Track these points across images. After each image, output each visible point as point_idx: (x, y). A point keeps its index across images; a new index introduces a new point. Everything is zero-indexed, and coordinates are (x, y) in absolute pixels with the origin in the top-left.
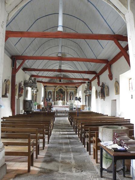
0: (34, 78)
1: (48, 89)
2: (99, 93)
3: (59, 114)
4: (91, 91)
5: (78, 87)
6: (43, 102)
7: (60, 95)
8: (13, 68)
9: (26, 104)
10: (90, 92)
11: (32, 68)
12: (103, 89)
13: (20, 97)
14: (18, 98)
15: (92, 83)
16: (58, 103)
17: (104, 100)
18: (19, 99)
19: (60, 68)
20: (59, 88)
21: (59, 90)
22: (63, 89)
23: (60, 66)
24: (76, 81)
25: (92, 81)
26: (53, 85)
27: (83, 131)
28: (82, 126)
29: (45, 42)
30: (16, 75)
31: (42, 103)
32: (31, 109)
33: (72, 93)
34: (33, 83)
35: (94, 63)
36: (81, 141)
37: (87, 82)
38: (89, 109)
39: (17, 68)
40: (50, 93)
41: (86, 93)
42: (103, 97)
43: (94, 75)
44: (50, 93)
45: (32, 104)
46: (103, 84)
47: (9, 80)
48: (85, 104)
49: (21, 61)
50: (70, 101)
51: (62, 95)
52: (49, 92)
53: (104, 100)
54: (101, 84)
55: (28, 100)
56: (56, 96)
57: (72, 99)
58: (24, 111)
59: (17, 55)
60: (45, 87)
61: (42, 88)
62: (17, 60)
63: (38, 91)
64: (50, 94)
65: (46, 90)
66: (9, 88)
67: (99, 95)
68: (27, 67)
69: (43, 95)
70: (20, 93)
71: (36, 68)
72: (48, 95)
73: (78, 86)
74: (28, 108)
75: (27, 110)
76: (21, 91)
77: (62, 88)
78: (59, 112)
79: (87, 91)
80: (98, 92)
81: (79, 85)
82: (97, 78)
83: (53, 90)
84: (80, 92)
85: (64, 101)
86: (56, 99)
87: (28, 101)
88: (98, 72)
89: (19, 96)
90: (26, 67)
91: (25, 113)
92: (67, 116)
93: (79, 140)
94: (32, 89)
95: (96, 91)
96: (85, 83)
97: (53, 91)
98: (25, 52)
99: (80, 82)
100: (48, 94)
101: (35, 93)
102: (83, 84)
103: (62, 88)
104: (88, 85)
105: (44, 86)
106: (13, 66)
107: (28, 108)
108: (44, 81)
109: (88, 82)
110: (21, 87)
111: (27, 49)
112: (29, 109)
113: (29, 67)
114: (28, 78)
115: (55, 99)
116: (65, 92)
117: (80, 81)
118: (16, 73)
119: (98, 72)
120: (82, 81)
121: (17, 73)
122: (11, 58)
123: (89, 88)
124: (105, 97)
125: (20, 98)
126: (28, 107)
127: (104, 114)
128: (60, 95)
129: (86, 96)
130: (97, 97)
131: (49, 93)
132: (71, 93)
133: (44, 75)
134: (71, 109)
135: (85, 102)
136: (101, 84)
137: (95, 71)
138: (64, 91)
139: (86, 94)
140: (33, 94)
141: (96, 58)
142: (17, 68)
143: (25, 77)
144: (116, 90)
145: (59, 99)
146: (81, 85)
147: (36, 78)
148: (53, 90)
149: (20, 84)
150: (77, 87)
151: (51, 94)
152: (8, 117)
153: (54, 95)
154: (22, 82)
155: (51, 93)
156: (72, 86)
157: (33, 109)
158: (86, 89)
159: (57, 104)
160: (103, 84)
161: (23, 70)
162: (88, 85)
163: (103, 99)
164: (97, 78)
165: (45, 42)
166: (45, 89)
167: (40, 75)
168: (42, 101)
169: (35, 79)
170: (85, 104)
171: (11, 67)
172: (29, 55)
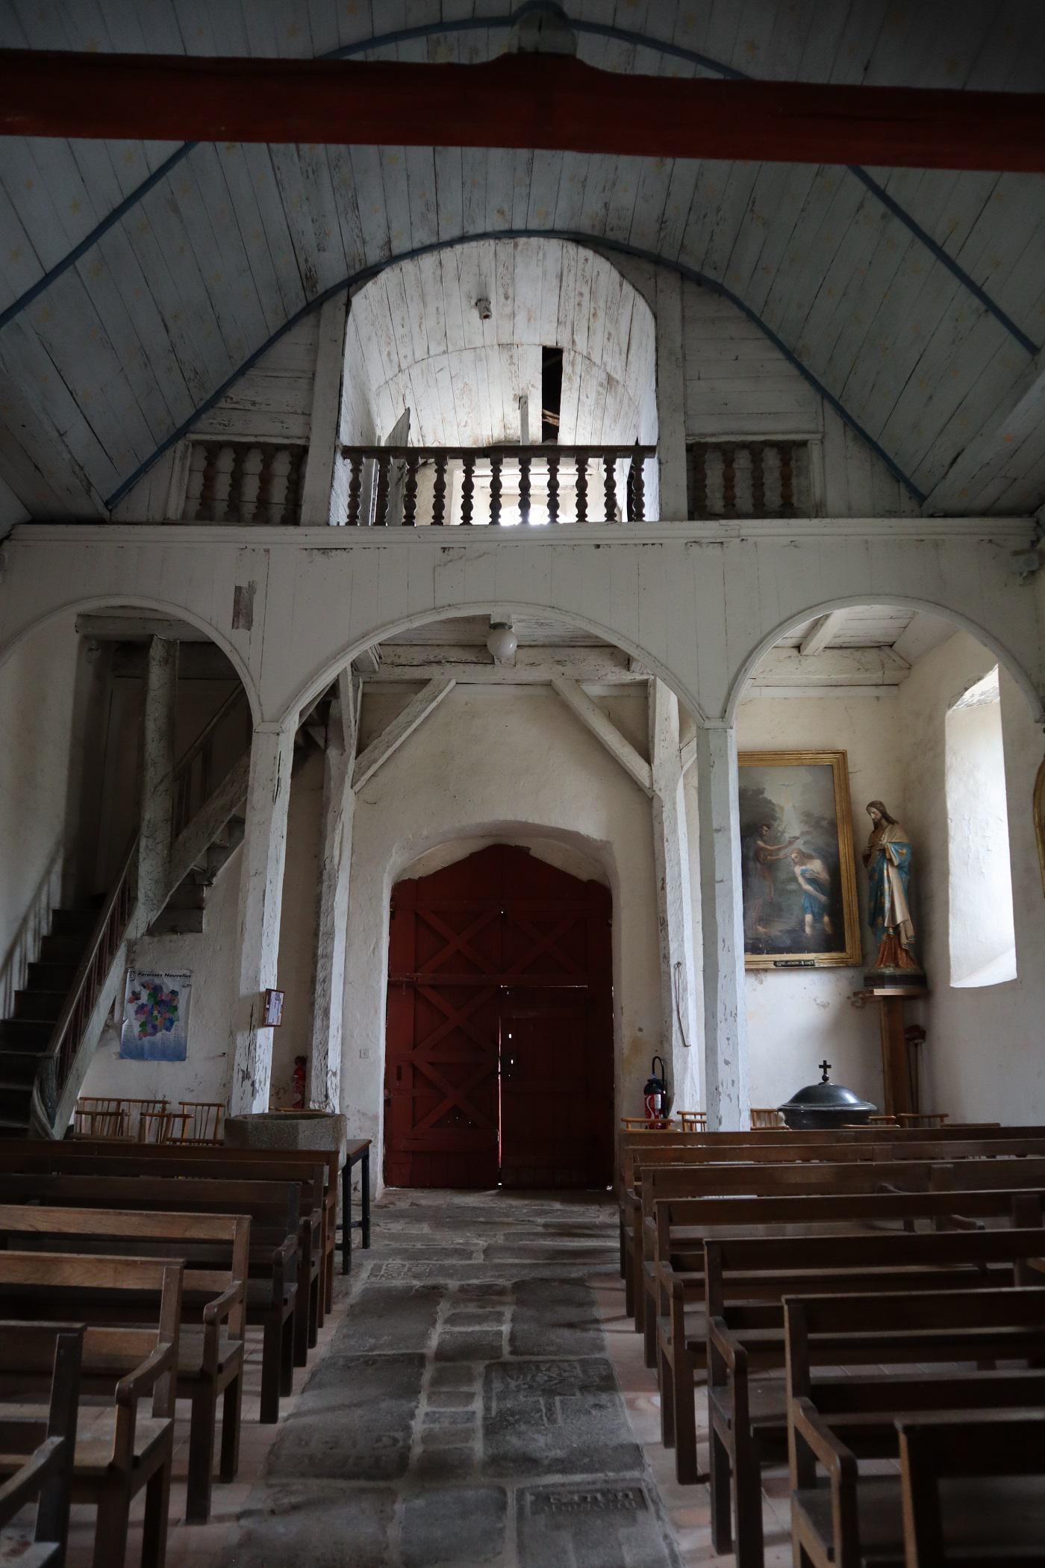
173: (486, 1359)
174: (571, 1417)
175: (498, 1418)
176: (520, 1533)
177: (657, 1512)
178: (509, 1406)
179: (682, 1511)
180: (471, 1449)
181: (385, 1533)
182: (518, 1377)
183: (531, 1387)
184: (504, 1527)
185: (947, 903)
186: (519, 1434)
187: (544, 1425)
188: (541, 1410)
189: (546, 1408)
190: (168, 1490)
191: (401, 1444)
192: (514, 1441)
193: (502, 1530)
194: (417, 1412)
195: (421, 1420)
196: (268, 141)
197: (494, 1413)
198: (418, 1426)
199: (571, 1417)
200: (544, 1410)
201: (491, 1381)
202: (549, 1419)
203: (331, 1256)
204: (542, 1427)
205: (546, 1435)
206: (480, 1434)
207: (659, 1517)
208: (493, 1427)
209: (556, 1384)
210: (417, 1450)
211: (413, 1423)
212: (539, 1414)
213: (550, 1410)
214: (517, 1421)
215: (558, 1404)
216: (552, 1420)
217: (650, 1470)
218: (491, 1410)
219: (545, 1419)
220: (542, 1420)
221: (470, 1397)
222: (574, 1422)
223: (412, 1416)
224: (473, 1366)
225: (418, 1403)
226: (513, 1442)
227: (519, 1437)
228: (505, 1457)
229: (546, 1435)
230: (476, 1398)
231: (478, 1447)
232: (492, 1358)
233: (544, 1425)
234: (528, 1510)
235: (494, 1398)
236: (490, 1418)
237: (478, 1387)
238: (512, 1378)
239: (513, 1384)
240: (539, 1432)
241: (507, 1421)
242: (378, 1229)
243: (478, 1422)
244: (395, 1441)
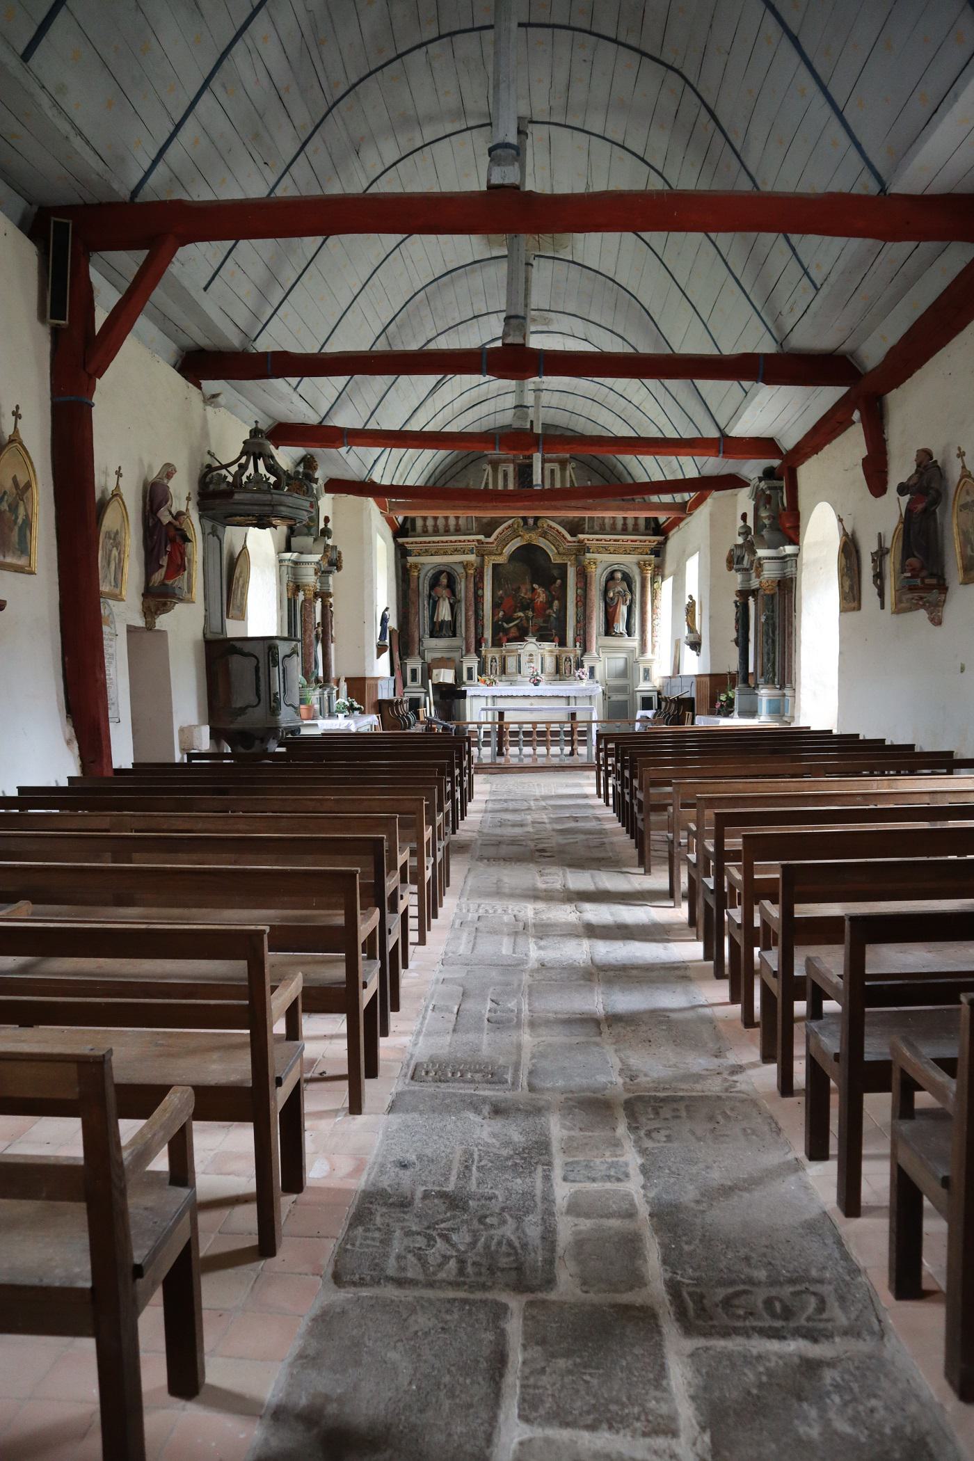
0: (299, 452)
1: (427, 552)
2: (880, 556)
3: (513, 750)
4: (789, 549)
5: (676, 523)
6: (386, 656)
7: (524, 593)
8: (56, 333)
9: (227, 673)
10: (783, 559)
11: (264, 345)
12: (929, 513)
13: (164, 608)
14: (139, 622)
15: (808, 473)
16: (511, 663)
17: (937, 621)
18: (150, 627)
19: (517, 340)
20: (700, 1323)
21: (513, 557)
22: (551, 551)
23: (515, 321)
24: (648, 460)
25: (806, 456)
26: (466, 515)
27: (732, 888)
28: (609, 746)
29: (362, 80)
30: (96, 398)
31: (381, 667)
32: (274, 711)
33: (627, 578)
34: (277, 486)
35: (855, 245)
36: (771, 1072)
37: (752, 469)
38: (778, 709)
39: (101, 317)
40: (444, 580)
41: (746, 571)
42: (929, 588)
43: (828, 396)
44: (444, 580)
45: (275, 671)
46: (928, 466)
47: (117, 494)
48: (733, 665)
49: (129, 262)
50: (611, 641)
51: (541, 596)
52: (441, 572)
53: (937, 621)
54: (901, 469)
55: (251, 633)
56: (496, 606)
57: (621, 627)
58: (206, 730)
59: (89, 199)
60: (400, 531)
61: (371, 542)
62: (95, 257)
63: (334, 563)
64: (445, 593)
65: (411, 559)
66: (27, 524)
67: (879, 577)
68: (223, 346)
69: (383, 595)
70: (158, 576)
71: (309, 346)
72: (424, 603)
73: (673, 515)
74: (242, 710)
75: (239, 723)
76: (164, 561)
77: (544, 535)
78: (514, 734)
79: (761, 553)
80: (868, 548)
81: (684, 510)
82: (856, 415)
83: (472, 558)
84: (693, 567)
85: (563, 643)
86: (497, 629)
87: (247, 648)
88: (872, 353)
89: (152, 603)
90: (203, 341)
91: (228, 749)
92: (584, 768)
93: (754, 1054)
94: (288, 549)
95: (850, 549)
96: (732, 482)
97: (466, 566)
98: (161, 167)
99: (692, 473)
100: (425, 588)
101: (310, 578)
102: (715, 499)
103: (542, 543)
104: (768, 499)
105: (390, 521)
106: (57, 313)
107: (242, 710)
108: (386, 482)
109: (769, 474)
110: (166, 519)
111: (183, 135)
112: (255, 718)
113: (234, 340)
114: (240, 447)
115: (488, 634)
116: (563, 568)
117: (689, 467)
118: (91, 389)
119: (872, 353)
120: (712, 465)
121: (99, 383)
122: (32, 235)
123: (776, 526)
124: (943, 588)
125: (163, 622)
126: (243, 695)
127: (957, 757)
128: (524, 593)
129: (744, 594)
130: (851, 598)
131: (435, 582)
132: (611, 577)
133: (390, 421)
134: (617, 709)
135: (735, 652)
136: (901, 469)
137: (846, 347)
138: (556, 559)
139: (747, 580)
140: (297, 587)
141: (873, 188)
142: (101, 317)
143: (205, 434)
144: (844, 597)
145: (514, 632)
146: (698, 502)
147: (317, 451)
148: (472, 558)
149: (154, 496)
150: (660, 530)
151: (453, 593)
152: (15, 793)
153: (478, 599)
154: (169, 471)
155: (451, 585)
156: (619, 515)
157: (286, 717)
158: (745, 532)
159: (504, 671)
160: (928, 466)
161: (179, 371)
162: (761, 499)
163: (922, 614)
164: (856, 415)
165: (362, 80)
166: (402, 553)
167: (345, 420)
168: (381, 649)
169: (308, 463)
170: (733, 665)
171: (42, 317)
172: (201, 193)
173: (554, 1303)
174: (443, 1154)
175: (533, 1161)
176: (519, 1055)
177: (411, 1058)
178: (519, 1181)
179: (199, 1441)
180: (564, 1126)
181: (621, 1060)
182: (499, 1243)
183: (482, 1219)
184: (531, 1060)
185: (387, 560)
186: (507, 1144)
187: (479, 1150)
188: (478, 1167)
189: (470, 1170)
190: (891, 1202)
191: (642, 1133)
192: (517, 1137)
193: (533, 1057)
194: (640, 1179)
195: (630, 1166)
196: (652, 482)
197: (540, 1168)
198: (632, 1159)
199: (443, 1154)
200: (474, 1168)
201: (543, 1238)
202: (472, 1155)
203: (669, 784)
204: (480, 1148)
205: (479, 1138)
206: (555, 1147)
207: (412, 1056)
208: (538, 1152)
209: (443, 1221)
210: (622, 1129)
211: (640, 1161)
212: (482, 1163)
213: (467, 1167)
214: (510, 1158)
215: (453, 1179)
216: (468, 1155)
217: (393, 1090)
218: (523, 1400)
219: (476, 1157)
220: (480, 1155)
221: (574, 1208)
222: (442, 1148)
223: (644, 1170)
224: (578, 1291)
225: (645, 1196)
226: (515, 1132)
227: (510, 1139)
228: (528, 1114)
229: (479, 1138)
230: (565, 1203)
231: (556, 1128)
232: (544, 1302)
233: (479, 1150)
234: (511, 1071)
235: (538, 1199)
236: (543, 1165)
237: (566, 1229)
238: (510, 1244)
239: (508, 1230)
240: (488, 1145)
241: (522, 1158)
242: (471, 483)
243: (558, 1160)
244: (649, 1134)
